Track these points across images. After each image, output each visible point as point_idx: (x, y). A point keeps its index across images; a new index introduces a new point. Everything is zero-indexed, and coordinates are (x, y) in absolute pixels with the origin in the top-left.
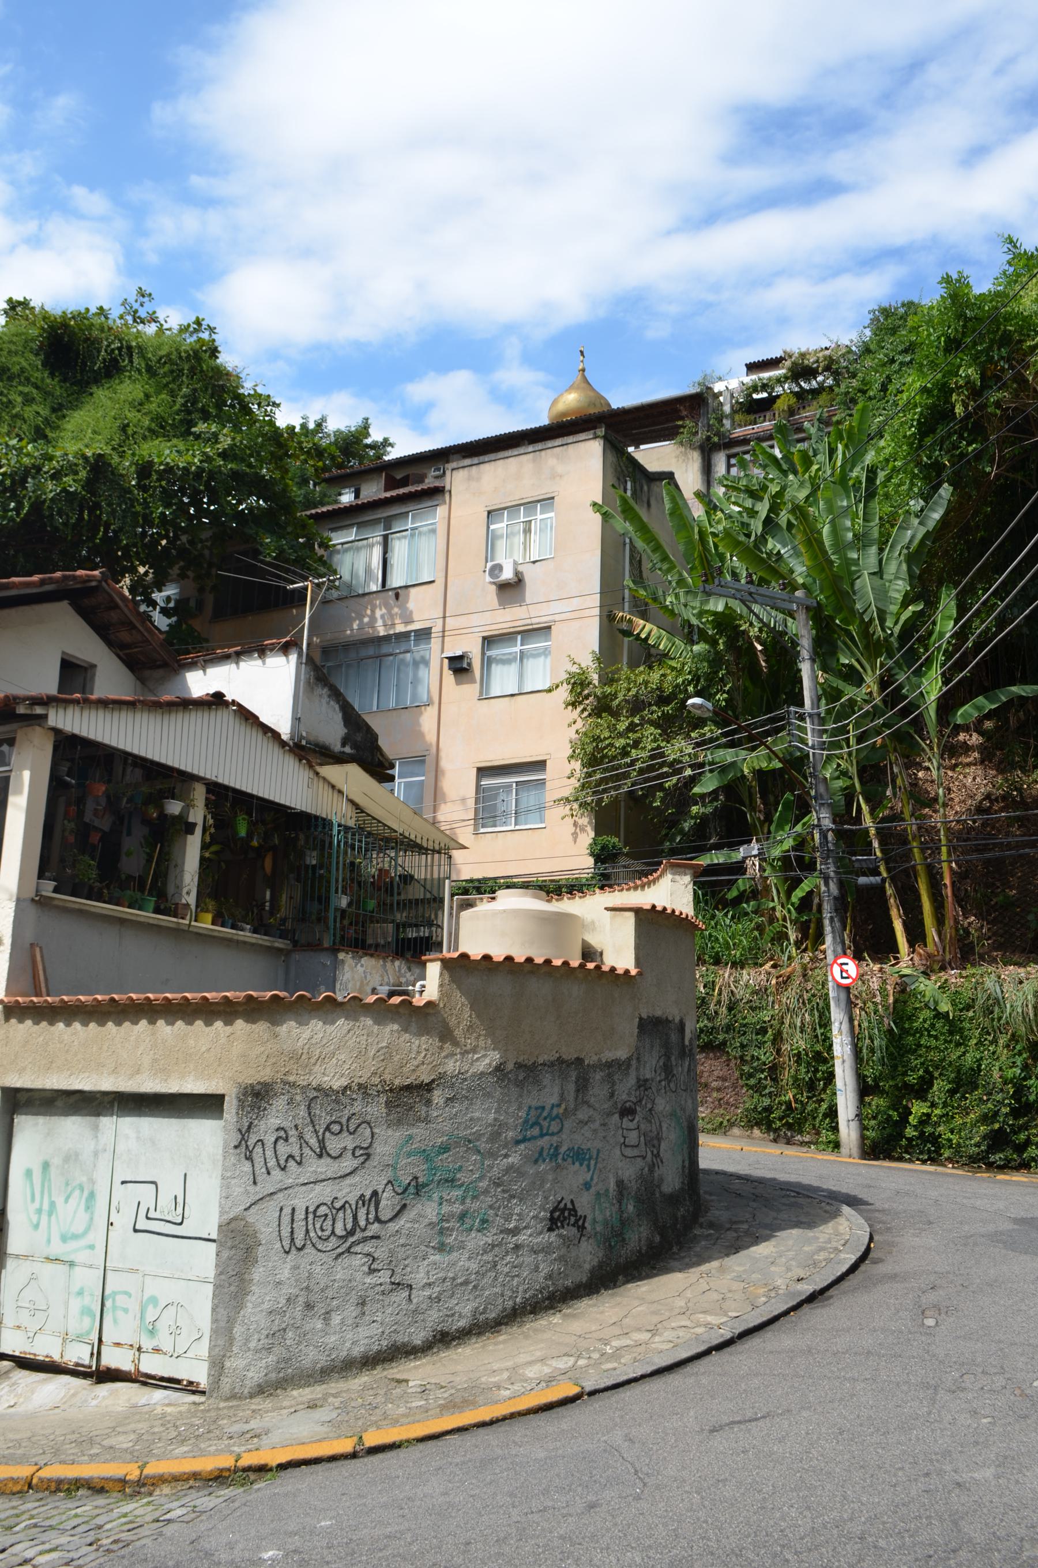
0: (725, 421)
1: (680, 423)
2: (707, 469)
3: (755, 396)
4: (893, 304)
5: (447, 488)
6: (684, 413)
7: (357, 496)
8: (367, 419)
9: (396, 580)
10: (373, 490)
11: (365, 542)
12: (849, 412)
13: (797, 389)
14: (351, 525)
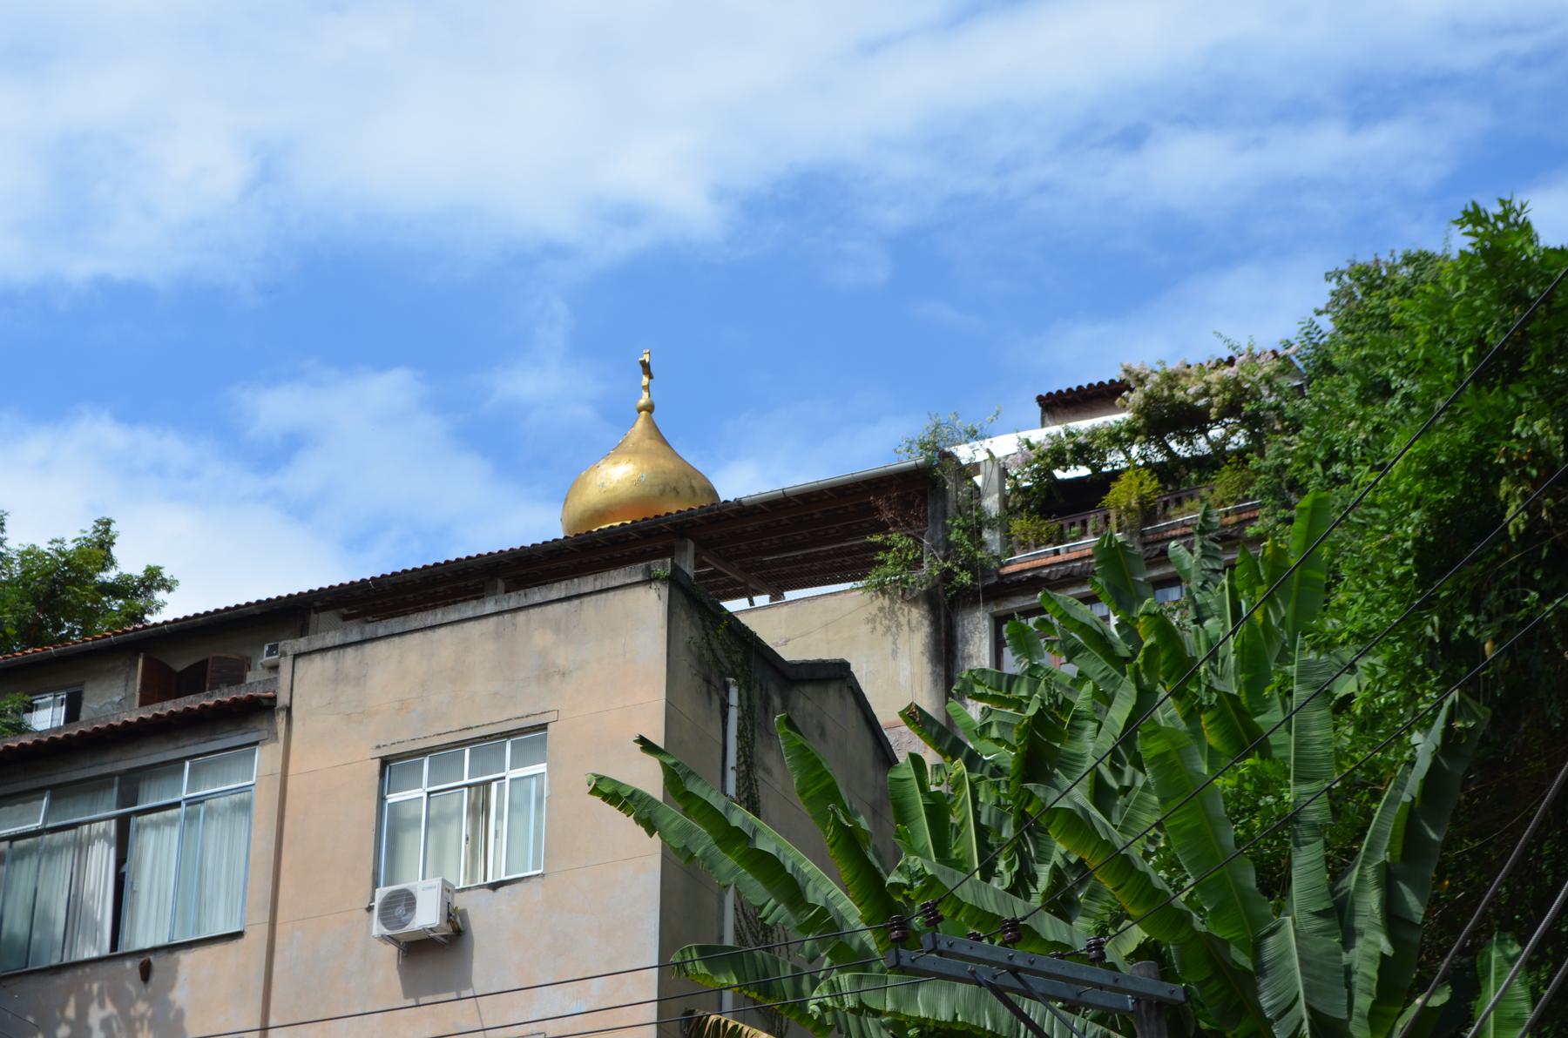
0: (986, 535)
1: (878, 538)
2: (945, 651)
3: (1059, 474)
4: (1385, 257)
5: (283, 700)
6: (888, 515)
7: (72, 716)
8: (109, 523)
9: (146, 933)
10: (114, 701)
11: (69, 834)
12: (1282, 513)
13: (1159, 458)
14: (37, 793)
